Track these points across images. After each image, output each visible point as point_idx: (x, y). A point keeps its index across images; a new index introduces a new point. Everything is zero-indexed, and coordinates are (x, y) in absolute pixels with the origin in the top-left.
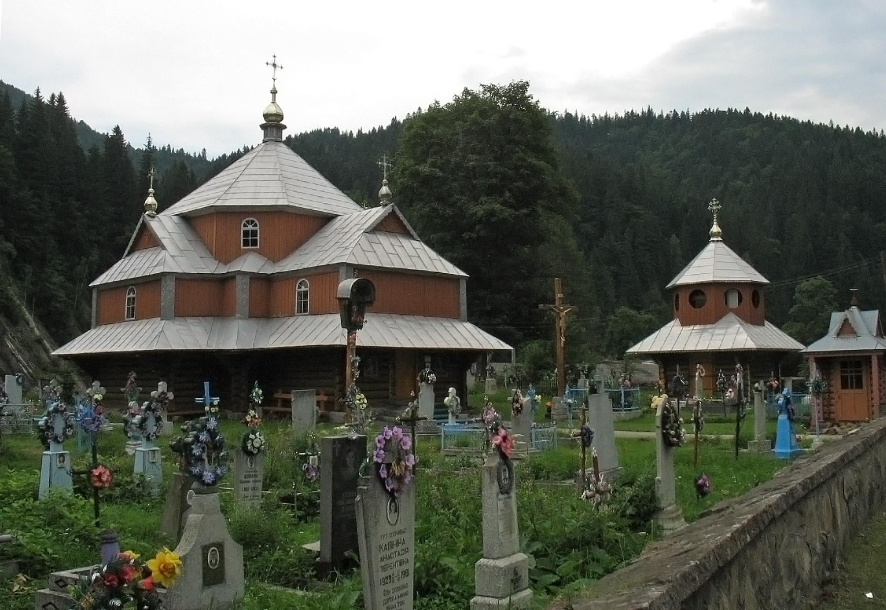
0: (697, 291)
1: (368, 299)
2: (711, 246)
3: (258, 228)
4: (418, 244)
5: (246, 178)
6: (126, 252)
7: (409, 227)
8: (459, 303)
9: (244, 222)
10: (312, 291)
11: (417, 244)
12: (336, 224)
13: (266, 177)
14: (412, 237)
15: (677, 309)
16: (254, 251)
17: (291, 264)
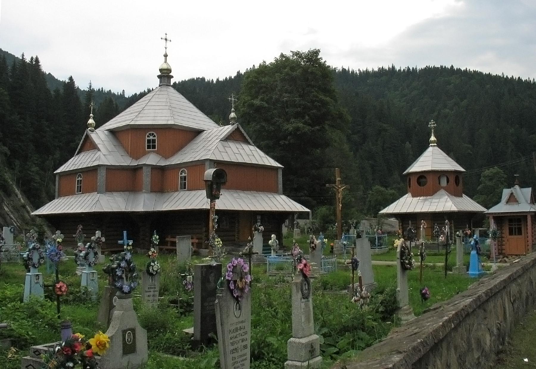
0: (422, 176)
1: (223, 181)
2: (430, 149)
3: (156, 138)
4: (253, 148)
5: (149, 107)
6: (76, 152)
7: (247, 138)
8: (277, 183)
9: (148, 134)
10: (189, 176)
11: (252, 148)
12: (204, 135)
14: (249, 143)
15: (410, 187)
16: (154, 152)
17: (176, 160)
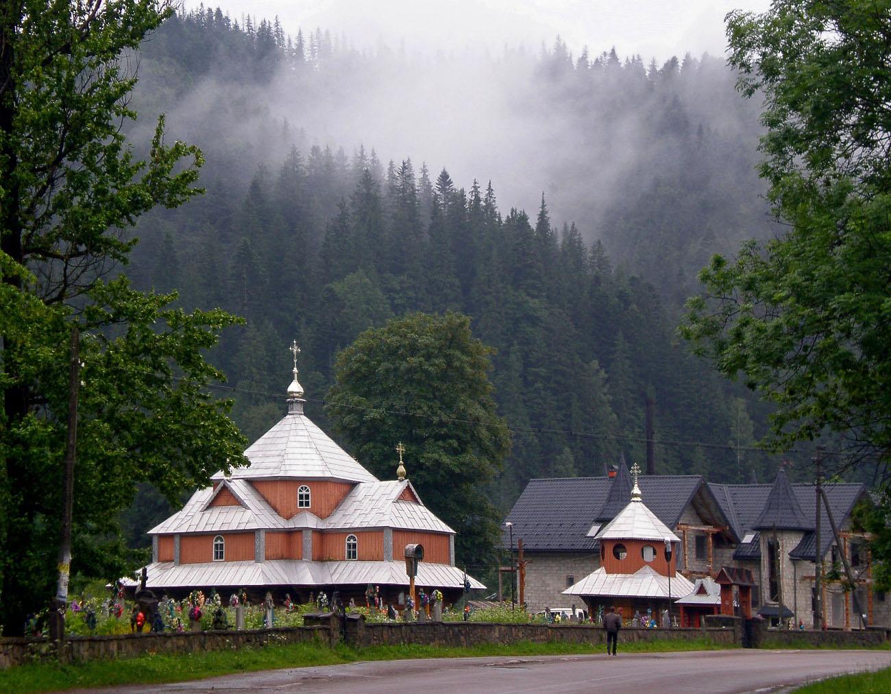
0: (620, 545)
2: (632, 505)
7: (417, 497)
13: (332, 456)
15: (603, 559)
